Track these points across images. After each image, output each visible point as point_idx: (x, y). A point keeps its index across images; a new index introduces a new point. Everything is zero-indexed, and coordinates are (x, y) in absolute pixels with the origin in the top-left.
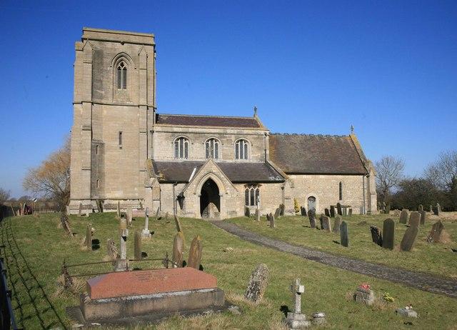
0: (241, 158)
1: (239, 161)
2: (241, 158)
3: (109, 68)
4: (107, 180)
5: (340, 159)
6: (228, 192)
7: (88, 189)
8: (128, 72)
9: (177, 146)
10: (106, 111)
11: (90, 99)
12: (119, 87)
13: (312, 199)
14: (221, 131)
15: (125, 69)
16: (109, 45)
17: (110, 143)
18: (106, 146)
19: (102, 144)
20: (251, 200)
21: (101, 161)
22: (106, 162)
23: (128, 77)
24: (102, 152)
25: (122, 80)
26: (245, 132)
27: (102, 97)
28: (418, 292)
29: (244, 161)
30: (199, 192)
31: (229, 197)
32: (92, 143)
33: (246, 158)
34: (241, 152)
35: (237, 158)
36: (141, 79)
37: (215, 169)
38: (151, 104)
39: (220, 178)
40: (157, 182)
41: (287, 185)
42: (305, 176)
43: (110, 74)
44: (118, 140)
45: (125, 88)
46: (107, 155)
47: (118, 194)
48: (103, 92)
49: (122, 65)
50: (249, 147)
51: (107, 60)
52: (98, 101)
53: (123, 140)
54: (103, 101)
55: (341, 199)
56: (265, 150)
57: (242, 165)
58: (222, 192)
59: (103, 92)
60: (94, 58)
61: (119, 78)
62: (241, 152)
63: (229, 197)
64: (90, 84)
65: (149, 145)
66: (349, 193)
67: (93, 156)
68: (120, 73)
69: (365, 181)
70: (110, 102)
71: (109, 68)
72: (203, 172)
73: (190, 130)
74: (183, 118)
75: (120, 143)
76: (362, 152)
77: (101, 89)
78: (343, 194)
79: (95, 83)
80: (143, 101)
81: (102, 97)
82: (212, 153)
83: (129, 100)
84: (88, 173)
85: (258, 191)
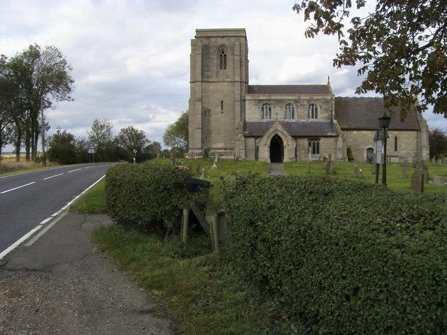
0: (313, 117)
2: (313, 117)
4: (213, 135)
7: (200, 141)
8: (228, 57)
11: (200, 79)
16: (213, 40)
19: (210, 111)
21: (209, 121)
22: (212, 122)
24: (210, 116)
25: (223, 64)
27: (209, 77)
30: (269, 143)
33: (316, 117)
37: (280, 128)
38: (244, 80)
41: (340, 139)
42: (364, 132)
43: (215, 60)
46: (213, 117)
47: (221, 145)
48: (209, 74)
49: (223, 53)
51: (212, 50)
54: (209, 80)
55: (396, 150)
57: (315, 123)
59: (209, 74)
60: (203, 50)
61: (221, 61)
64: (200, 68)
67: (203, 119)
70: (214, 80)
72: (271, 130)
81: (209, 77)
84: (200, 131)
85: (318, 143)
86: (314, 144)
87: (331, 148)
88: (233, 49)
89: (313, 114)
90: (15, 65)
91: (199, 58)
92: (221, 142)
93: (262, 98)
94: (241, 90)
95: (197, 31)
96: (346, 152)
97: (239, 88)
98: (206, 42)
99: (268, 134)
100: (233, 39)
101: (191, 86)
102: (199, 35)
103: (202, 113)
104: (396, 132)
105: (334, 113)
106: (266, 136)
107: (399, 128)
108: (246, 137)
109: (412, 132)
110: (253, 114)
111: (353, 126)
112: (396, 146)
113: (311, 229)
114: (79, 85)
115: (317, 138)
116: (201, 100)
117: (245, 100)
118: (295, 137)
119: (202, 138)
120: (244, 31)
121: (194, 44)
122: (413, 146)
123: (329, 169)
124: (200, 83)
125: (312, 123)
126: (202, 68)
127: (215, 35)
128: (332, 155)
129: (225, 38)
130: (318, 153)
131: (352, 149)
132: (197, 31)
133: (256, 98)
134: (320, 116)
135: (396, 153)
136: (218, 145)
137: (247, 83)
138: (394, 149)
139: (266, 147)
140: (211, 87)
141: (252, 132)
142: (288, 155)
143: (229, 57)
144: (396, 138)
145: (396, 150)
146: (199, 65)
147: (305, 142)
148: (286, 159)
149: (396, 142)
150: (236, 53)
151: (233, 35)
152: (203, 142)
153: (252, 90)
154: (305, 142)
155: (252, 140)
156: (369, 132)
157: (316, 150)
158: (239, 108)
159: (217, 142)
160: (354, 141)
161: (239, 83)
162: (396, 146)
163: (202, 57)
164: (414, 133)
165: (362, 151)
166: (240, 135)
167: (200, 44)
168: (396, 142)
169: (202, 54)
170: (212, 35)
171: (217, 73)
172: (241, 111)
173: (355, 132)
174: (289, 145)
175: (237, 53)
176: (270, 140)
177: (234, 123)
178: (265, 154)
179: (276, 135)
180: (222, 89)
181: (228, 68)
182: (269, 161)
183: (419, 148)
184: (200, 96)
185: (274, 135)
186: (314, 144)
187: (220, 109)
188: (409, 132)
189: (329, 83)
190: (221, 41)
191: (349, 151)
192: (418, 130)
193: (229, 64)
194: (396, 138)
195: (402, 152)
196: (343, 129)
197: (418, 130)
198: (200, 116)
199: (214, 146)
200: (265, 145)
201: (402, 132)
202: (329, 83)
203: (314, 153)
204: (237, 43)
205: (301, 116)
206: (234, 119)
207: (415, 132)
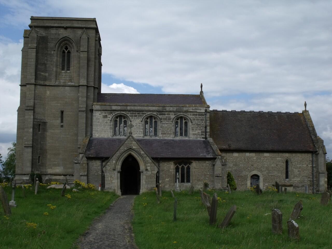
1: (179, 138)
2: (181, 134)
3: (52, 52)
4: (48, 156)
6: (149, 168)
7: (29, 164)
8: (72, 55)
10: (48, 92)
11: (33, 81)
12: (63, 69)
13: (255, 177)
15: (69, 52)
16: (53, 31)
17: (53, 122)
18: (48, 124)
19: (45, 123)
21: (44, 138)
22: (48, 139)
23: (72, 60)
24: (45, 130)
25: (66, 63)
27: (45, 79)
29: (187, 138)
30: (119, 167)
32: (34, 121)
33: (186, 135)
36: (81, 61)
38: (92, 84)
39: (140, 154)
40: (85, 159)
41: (218, 163)
42: (248, 154)
43: (55, 58)
44: (60, 119)
45: (69, 70)
46: (49, 133)
47: (58, 170)
48: (47, 74)
49: (66, 48)
50: (190, 124)
51: (51, 45)
52: (42, 83)
53: (64, 119)
54: (47, 83)
55: (287, 177)
56: (206, 127)
57: (184, 141)
58: (142, 167)
59: (47, 74)
60: (38, 43)
61: (63, 60)
64: (33, 67)
65: (89, 124)
66: (296, 171)
67: (34, 134)
68: (64, 56)
70: (53, 83)
71: (52, 52)
72: (123, 149)
75: (62, 121)
77: (45, 71)
78: (289, 173)
79: (39, 66)
81: (45, 79)
83: (70, 81)
84: (30, 150)
85: (188, 168)
86: (183, 168)
87: (205, 175)
88: (78, 43)
89: (181, 129)
90: (191, 163)
91: (33, 54)
92: (58, 165)
93: (114, 108)
94: (87, 97)
95: (32, 19)
96: (226, 180)
97: (85, 94)
98: (42, 33)
99: (118, 154)
100: (79, 32)
101: (21, 90)
102: (35, 24)
103: (34, 125)
104: (287, 155)
105: (208, 130)
106: (115, 157)
107: (291, 148)
108: (89, 158)
109: (306, 154)
110: (102, 129)
111: (233, 147)
115: (187, 161)
116: (33, 109)
117: (92, 111)
118: (157, 160)
119: (33, 159)
120: (94, 21)
121: (27, 36)
122: (308, 172)
123: (318, 185)
124: (33, 87)
125: (180, 141)
126: (36, 66)
127: (56, 25)
128: (81, 174)
129: (69, 30)
130: (188, 181)
131: (233, 176)
132: (32, 19)
133: (108, 108)
134: (191, 132)
135: (287, 182)
136: (54, 168)
137: (99, 88)
138: (284, 176)
139: (116, 172)
140: (48, 92)
141: (97, 153)
142: (146, 184)
143: (74, 54)
144: (287, 162)
145: (287, 177)
146: (32, 62)
147: (171, 166)
148: (143, 189)
150: (82, 49)
151: (80, 26)
152: (33, 164)
153: (102, 98)
154: (171, 166)
155: (98, 163)
156: (253, 155)
157: (185, 177)
158: (84, 121)
159: (55, 165)
160: (235, 165)
161: (86, 87)
163: (37, 53)
164: (308, 157)
165: (245, 178)
166: (81, 155)
167: (35, 35)
169: (37, 48)
170: (53, 25)
171: (57, 76)
172: (86, 124)
173: (236, 155)
174: (147, 169)
175: (84, 48)
176: (120, 163)
177: (77, 140)
178: (114, 182)
179: (130, 156)
180: (62, 95)
181: (71, 68)
182: (119, 192)
183: (315, 175)
184: (32, 104)
185: (126, 155)
186: (183, 168)
187: (59, 121)
188: (303, 154)
189: (202, 92)
190: (63, 33)
191: (229, 176)
192: (314, 153)
193: (74, 62)
194: (287, 162)
195: (295, 180)
196: (222, 150)
197: (314, 153)
198: (31, 130)
199: (50, 171)
200: (114, 170)
201: (294, 155)
202: (202, 92)
203: (183, 181)
204: (84, 36)
205: (167, 132)
206: (77, 135)
207: (310, 155)
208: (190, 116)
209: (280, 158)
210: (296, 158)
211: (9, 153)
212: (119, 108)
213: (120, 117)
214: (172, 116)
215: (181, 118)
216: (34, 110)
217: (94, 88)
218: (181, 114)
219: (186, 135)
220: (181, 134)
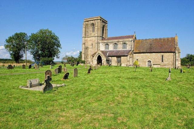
0: (124, 48)
1: (124, 49)
5: (166, 46)
9: (114, 46)
10: (89, 39)
13: (149, 61)
14: (118, 41)
16: (90, 22)
19: (88, 47)
20: (119, 62)
24: (88, 49)
26: (125, 40)
28: (32, 56)
29: (126, 49)
30: (96, 59)
31: (104, 60)
33: (126, 48)
34: (125, 46)
35: (123, 48)
37: (100, 53)
42: (147, 54)
55: (162, 61)
57: (126, 50)
62: (125, 46)
63: (104, 60)
65: (98, 47)
69: (174, 54)
73: (109, 41)
74: (112, 38)
76: (177, 43)
80: (97, 35)
81: (88, 35)
82: (125, 47)
93: (105, 42)
104: (162, 54)
105: (133, 46)
112: (162, 60)
113: (62, 124)
114: (5, 40)
122: (172, 60)
144: (162, 56)
149: (162, 58)
162: (162, 60)
168: (162, 58)
182: (177, 39)
204: (97, 22)
208: (127, 42)
209: (160, 55)
210: (166, 55)
211: (57, 62)
212: (106, 42)
213: (107, 44)
214: (121, 43)
215: (124, 43)
216: (85, 44)
217: (100, 37)
218: (124, 42)
219: (126, 48)
220: (124, 48)
